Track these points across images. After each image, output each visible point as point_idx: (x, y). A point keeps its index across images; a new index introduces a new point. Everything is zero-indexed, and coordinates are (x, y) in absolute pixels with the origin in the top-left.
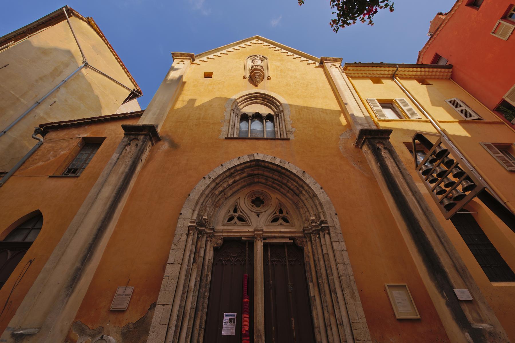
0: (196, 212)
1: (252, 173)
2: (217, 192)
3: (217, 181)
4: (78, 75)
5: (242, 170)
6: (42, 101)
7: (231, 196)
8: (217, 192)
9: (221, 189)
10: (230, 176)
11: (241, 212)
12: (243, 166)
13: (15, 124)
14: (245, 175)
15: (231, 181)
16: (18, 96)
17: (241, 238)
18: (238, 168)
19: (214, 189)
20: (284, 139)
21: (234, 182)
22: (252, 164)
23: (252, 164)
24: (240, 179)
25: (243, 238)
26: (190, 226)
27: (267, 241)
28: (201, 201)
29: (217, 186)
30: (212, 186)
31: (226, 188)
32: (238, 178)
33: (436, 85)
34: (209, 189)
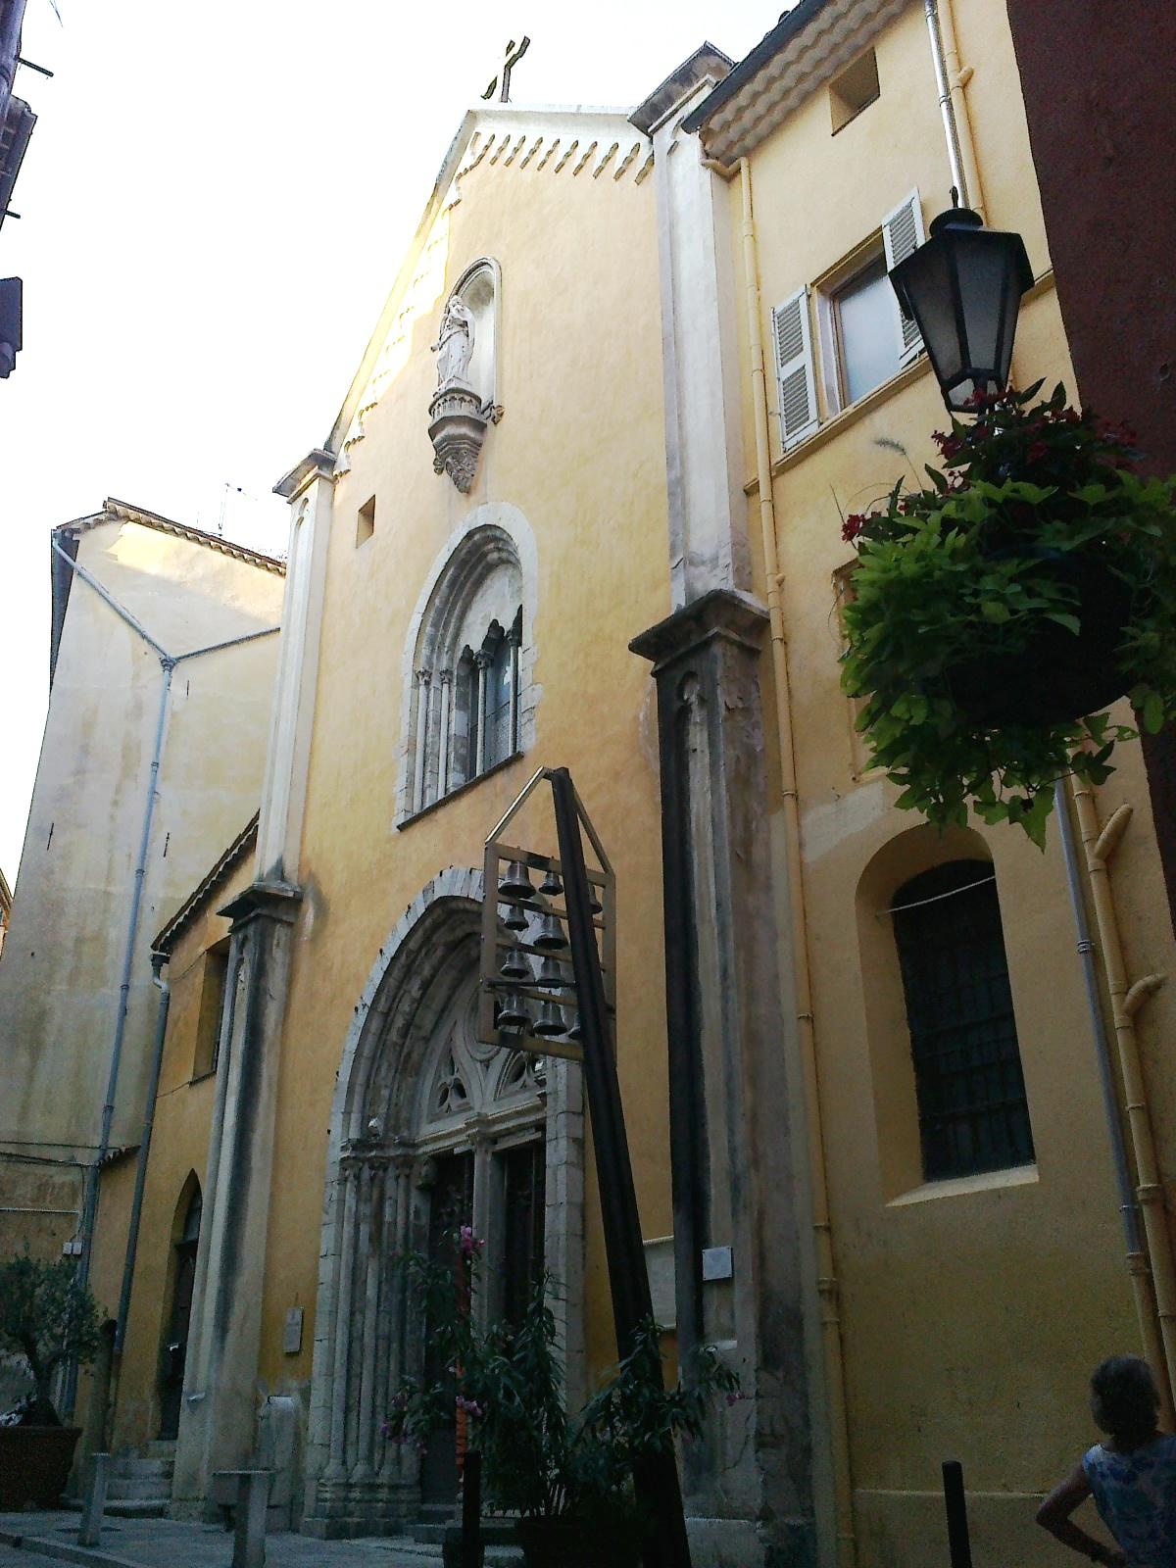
0: (355, 1117)
1: (452, 938)
2: (394, 1036)
3: (382, 1006)
4: (174, 715)
5: (427, 939)
6: (143, 862)
7: (437, 1024)
8: (394, 1036)
9: (399, 1022)
10: (408, 973)
11: (440, 1077)
12: (420, 933)
13: (135, 919)
14: (439, 952)
15: (414, 988)
16: (102, 887)
17: (453, 1150)
18: (412, 945)
19: (385, 1029)
20: (932, 357)
21: (425, 986)
22: (435, 916)
23: (435, 916)
24: (436, 970)
25: (457, 1151)
26: (343, 1160)
27: (499, 1147)
28: (361, 1079)
29: (389, 1019)
30: (375, 1025)
31: (413, 1015)
32: (427, 971)
33: (462, 712)
34: (371, 1039)
